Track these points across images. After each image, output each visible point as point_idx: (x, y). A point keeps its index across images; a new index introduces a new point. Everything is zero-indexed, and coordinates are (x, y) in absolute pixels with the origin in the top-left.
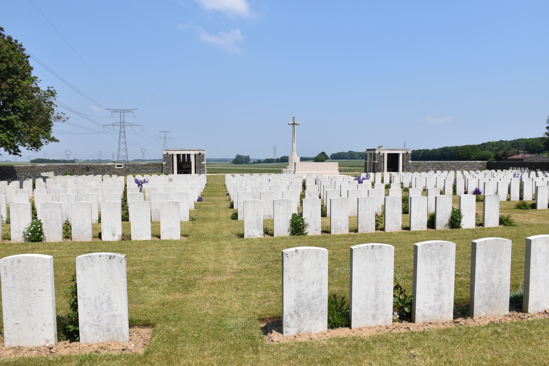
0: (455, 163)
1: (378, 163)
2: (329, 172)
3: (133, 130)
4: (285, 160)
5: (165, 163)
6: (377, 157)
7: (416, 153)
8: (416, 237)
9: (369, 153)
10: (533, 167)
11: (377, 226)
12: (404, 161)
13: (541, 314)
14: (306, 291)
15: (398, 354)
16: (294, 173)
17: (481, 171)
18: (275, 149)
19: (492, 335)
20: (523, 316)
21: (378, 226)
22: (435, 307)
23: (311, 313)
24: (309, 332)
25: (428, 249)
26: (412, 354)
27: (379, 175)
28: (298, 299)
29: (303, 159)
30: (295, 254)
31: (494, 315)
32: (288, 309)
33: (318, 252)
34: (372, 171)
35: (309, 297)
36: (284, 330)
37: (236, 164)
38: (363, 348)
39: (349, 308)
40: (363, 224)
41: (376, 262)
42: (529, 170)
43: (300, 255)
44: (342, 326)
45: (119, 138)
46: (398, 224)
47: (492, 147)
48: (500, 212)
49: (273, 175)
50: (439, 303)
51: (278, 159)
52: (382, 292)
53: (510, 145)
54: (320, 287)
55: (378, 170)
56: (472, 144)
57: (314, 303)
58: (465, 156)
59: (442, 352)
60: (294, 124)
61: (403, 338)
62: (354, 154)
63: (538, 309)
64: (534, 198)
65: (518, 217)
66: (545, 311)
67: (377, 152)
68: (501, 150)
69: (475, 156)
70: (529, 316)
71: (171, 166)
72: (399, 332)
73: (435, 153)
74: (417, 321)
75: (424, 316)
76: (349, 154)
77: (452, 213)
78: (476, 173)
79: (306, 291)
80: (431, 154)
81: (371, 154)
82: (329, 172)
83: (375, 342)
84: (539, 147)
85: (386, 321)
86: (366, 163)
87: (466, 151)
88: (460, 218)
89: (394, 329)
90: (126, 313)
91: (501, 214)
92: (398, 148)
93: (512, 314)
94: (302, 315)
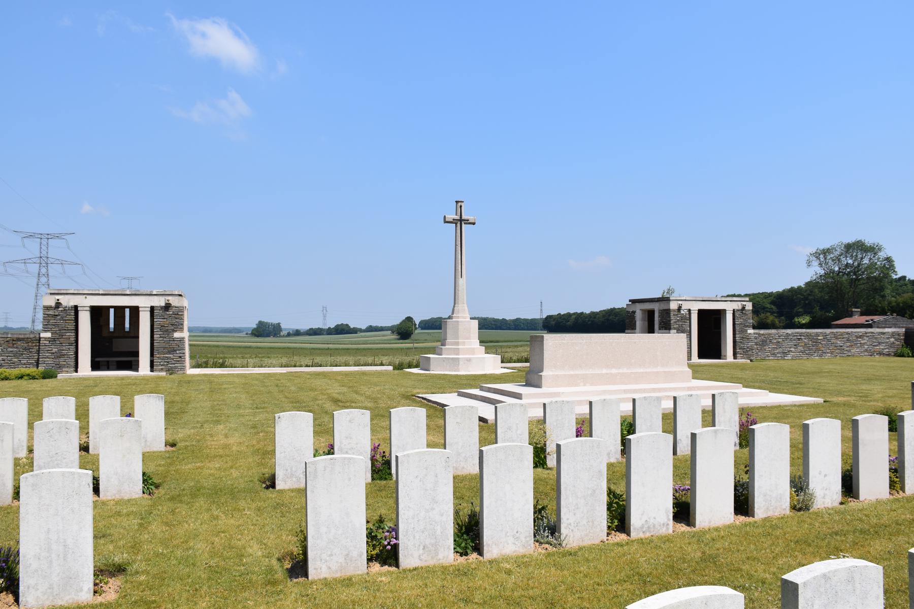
0: (842, 334)
2: (660, 369)
3: (64, 272)
5: (48, 335)
7: (564, 319)
12: (737, 328)
18: (325, 311)
37: (258, 336)
45: (35, 286)
51: (329, 328)
60: (460, 222)
71: (71, 344)
73: (595, 318)
80: (589, 321)
82: (660, 369)
90: (91, 544)
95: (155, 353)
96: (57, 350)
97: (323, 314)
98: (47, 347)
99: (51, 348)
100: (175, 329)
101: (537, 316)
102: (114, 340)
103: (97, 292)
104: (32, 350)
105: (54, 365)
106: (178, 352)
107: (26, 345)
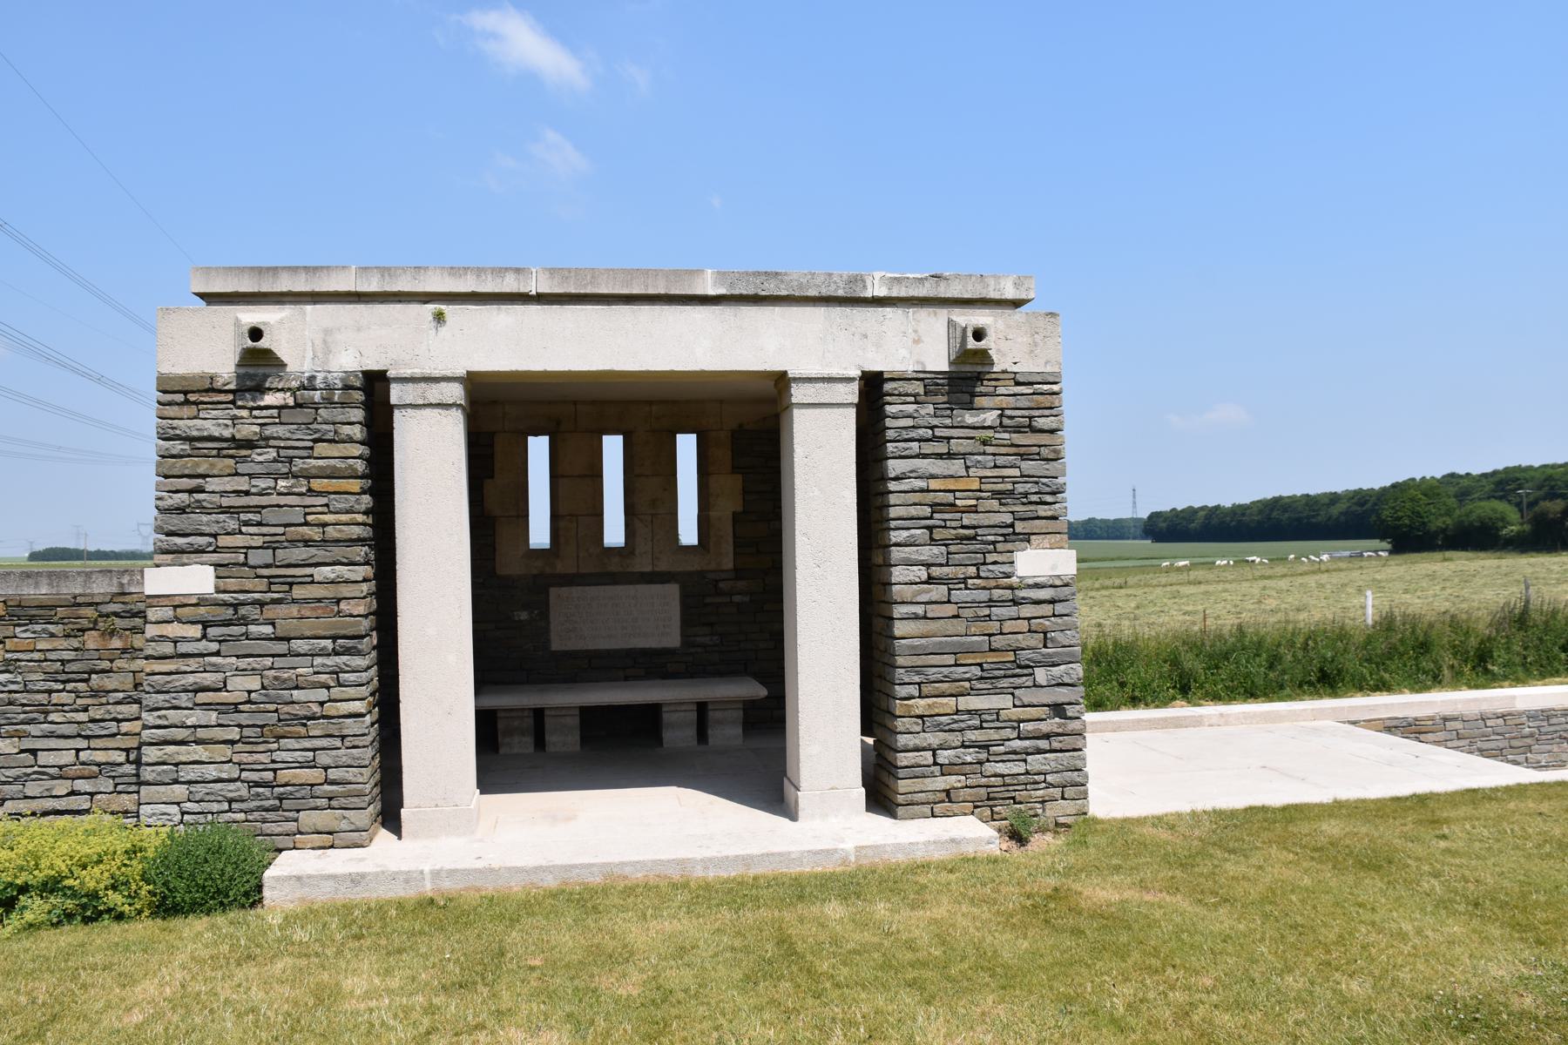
5: (197, 579)
7: (1183, 518)
58: (1407, 522)
71: (344, 643)
73: (1243, 515)
80: (1232, 521)
87: (1408, 505)
95: (901, 691)
96: (254, 683)
98: (193, 664)
99: (217, 669)
100: (1020, 527)
101: (1126, 514)
102: (553, 591)
103: (509, 285)
104: (109, 682)
105: (244, 792)
106: (1041, 675)
107: (63, 648)
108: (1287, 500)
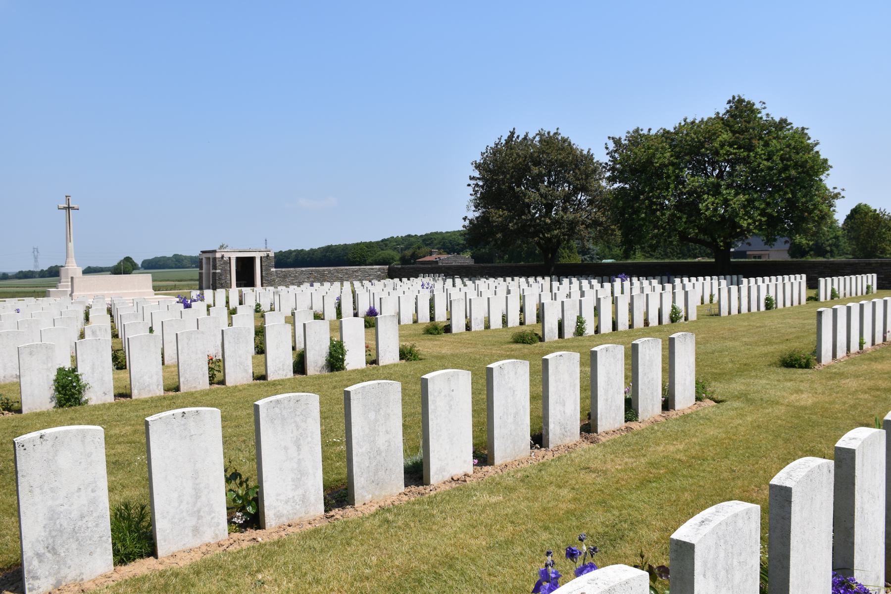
1: (221, 274)
2: (136, 291)
4: (54, 273)
6: (218, 263)
7: (285, 256)
8: (275, 390)
9: (206, 258)
10: (450, 272)
11: (212, 378)
13: (447, 483)
14: (66, 507)
15: (237, 585)
16: (71, 295)
17: (379, 281)
18: (36, 253)
19: (380, 526)
20: (423, 491)
21: (213, 378)
22: (296, 498)
23: (79, 544)
24: (79, 579)
25: (276, 408)
26: (259, 581)
27: (221, 293)
28: (53, 524)
29: (88, 271)
30: (39, 443)
31: (385, 496)
32: (32, 545)
33: (84, 435)
34: (211, 286)
35: (72, 516)
36: (27, 586)
38: (177, 588)
39: (152, 523)
40: (188, 376)
41: (190, 439)
42: (444, 277)
43: (50, 443)
44: (141, 557)
46: (246, 371)
47: (397, 245)
48: (401, 341)
49: (31, 301)
50: (300, 492)
51: (42, 271)
52: (205, 488)
53: (421, 241)
54: (92, 495)
55: (222, 284)
56: (368, 241)
57: (84, 526)
59: (306, 567)
60: (69, 208)
61: (245, 557)
62: (182, 260)
63: (443, 477)
64: (449, 318)
65: (426, 347)
66: (452, 479)
67: (218, 255)
68: (409, 248)
69: (372, 258)
70: (431, 489)
72: (239, 548)
73: (313, 254)
74: (268, 525)
75: (279, 516)
76: (174, 260)
77: (330, 348)
78: (372, 285)
79: (66, 507)
80: (308, 258)
81: (208, 259)
82: (136, 291)
83: (198, 573)
84: (459, 244)
85: (216, 535)
86: (201, 274)
88: (343, 355)
89: (231, 545)
91: (402, 343)
92: (253, 249)
93: (409, 490)
94: (62, 552)
97: (34, 256)
108: (334, 247)
